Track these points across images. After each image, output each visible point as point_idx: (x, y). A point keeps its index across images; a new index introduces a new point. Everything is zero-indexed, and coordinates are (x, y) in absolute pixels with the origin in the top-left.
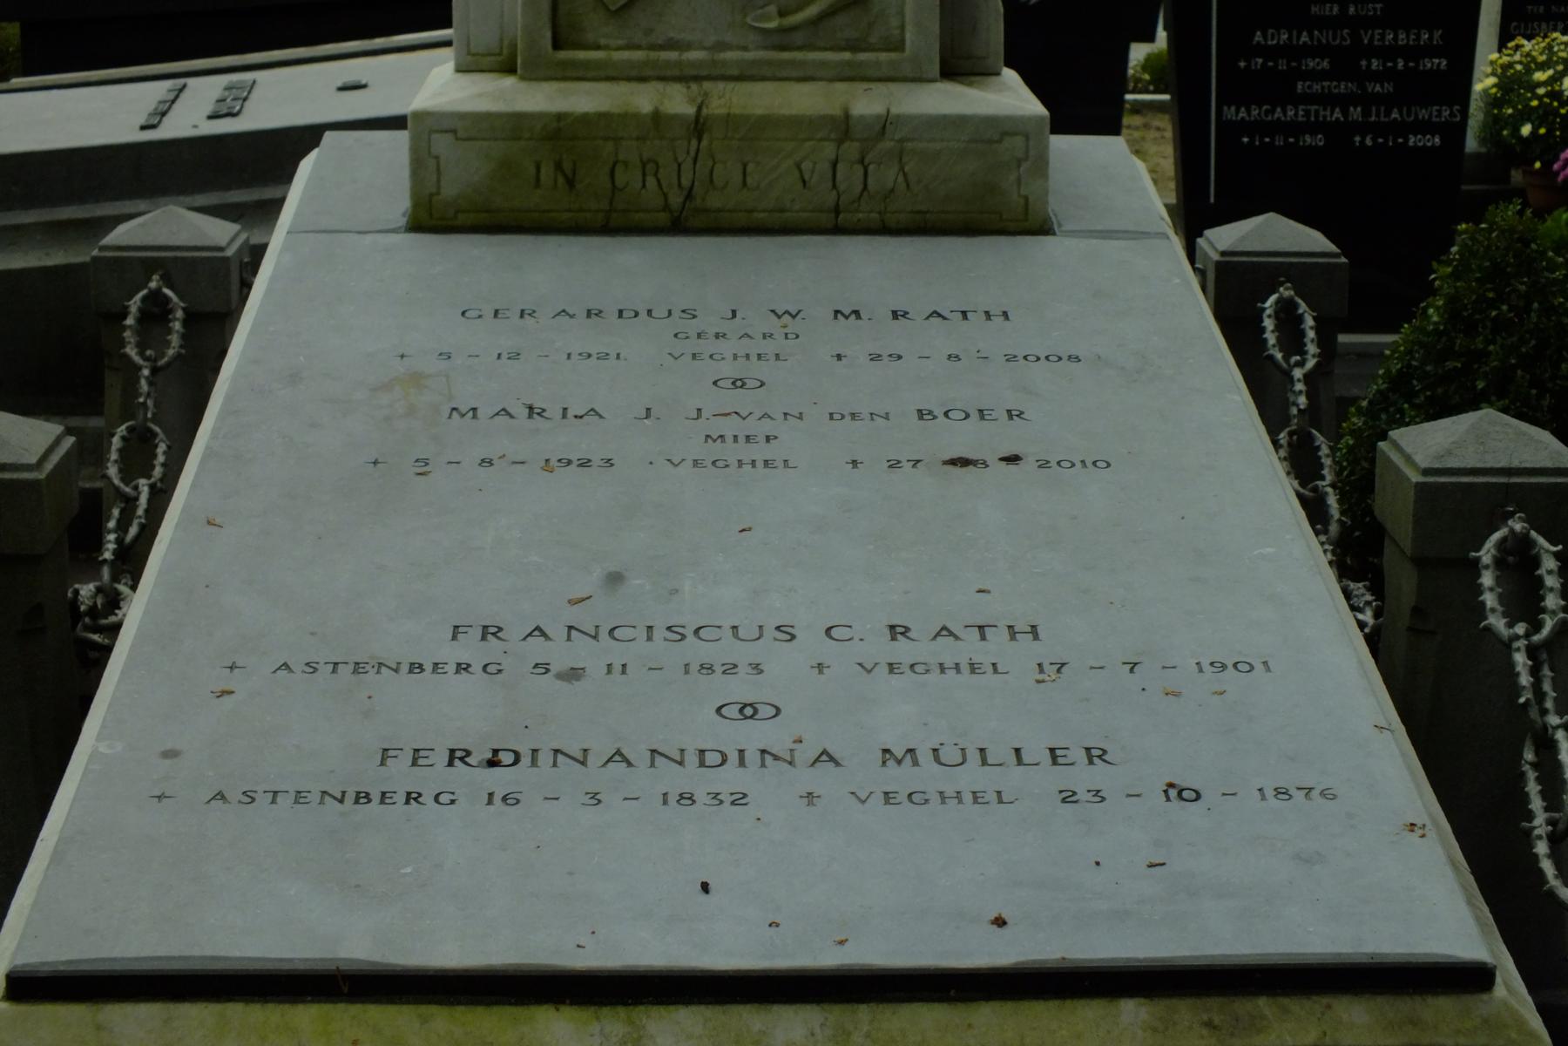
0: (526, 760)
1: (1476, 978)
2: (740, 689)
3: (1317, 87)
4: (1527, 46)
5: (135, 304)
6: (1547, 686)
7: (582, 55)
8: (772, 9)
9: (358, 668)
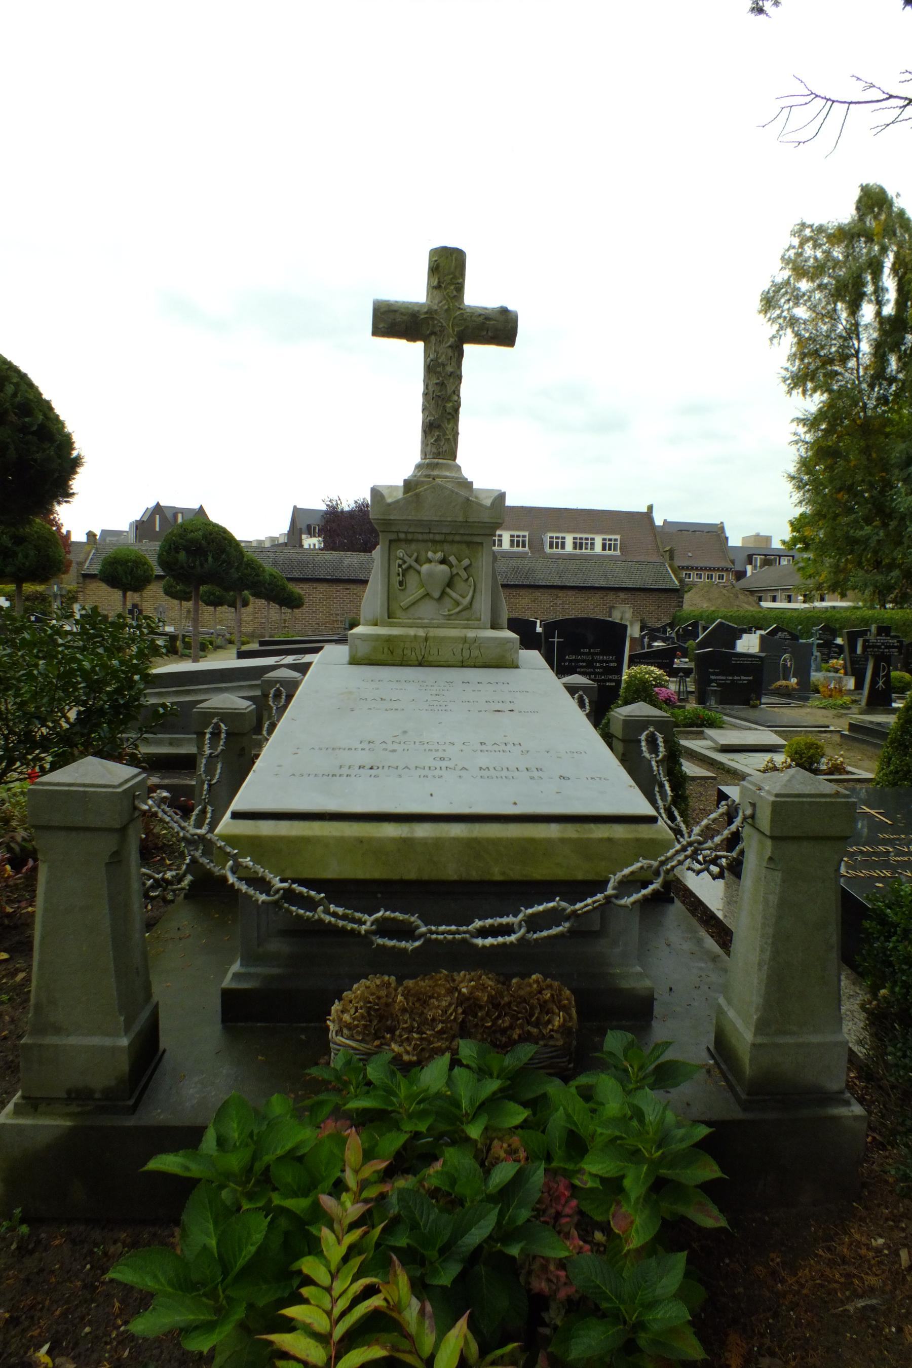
0: (381, 768)
1: (652, 820)
2: (440, 754)
3: (582, 670)
4: (635, 668)
5: (272, 691)
6: (661, 772)
7: (395, 620)
8: (446, 609)
9: (333, 749)
